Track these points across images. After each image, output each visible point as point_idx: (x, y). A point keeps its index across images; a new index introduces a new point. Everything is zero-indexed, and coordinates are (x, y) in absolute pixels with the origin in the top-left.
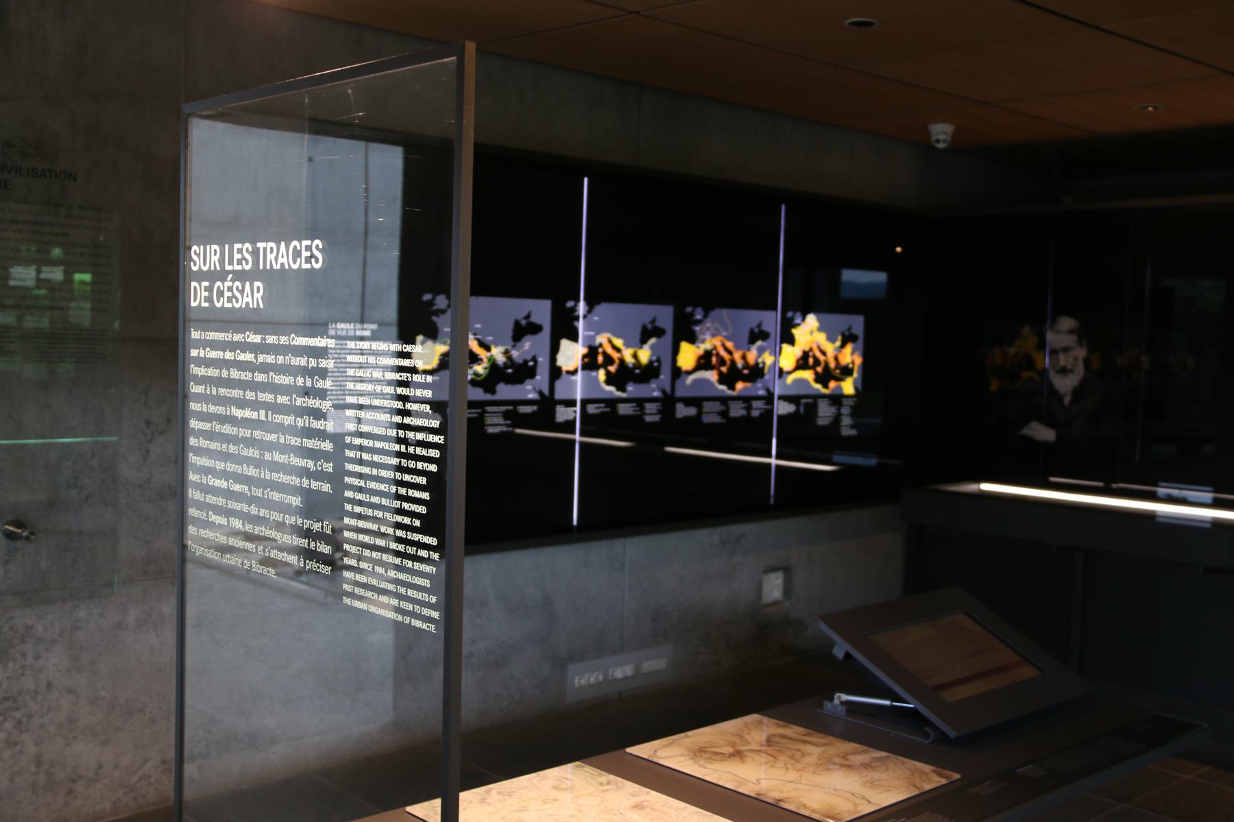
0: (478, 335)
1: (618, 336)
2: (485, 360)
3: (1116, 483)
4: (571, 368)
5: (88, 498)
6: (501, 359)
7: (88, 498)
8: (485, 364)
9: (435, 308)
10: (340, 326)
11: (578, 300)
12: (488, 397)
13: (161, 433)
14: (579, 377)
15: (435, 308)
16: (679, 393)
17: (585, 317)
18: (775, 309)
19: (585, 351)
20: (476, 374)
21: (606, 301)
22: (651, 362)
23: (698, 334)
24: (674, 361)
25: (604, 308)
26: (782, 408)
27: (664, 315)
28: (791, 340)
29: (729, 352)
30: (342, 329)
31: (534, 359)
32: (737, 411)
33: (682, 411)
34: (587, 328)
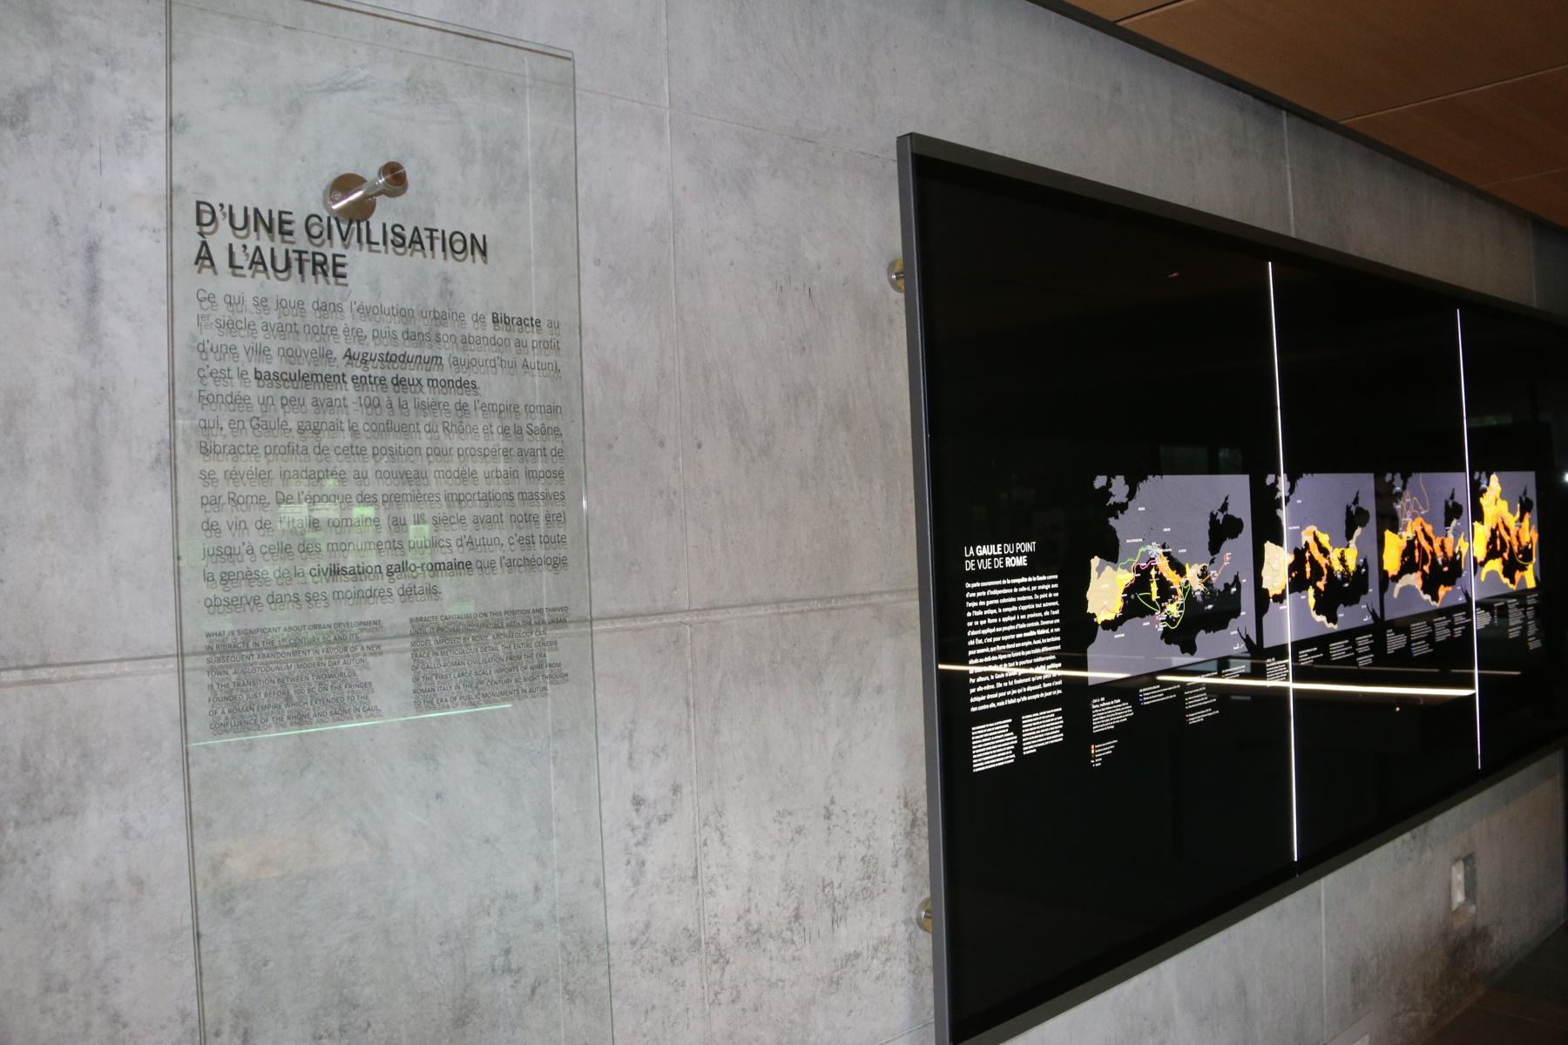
0: (1168, 548)
1: (1323, 532)
2: (1180, 592)
3: (1174, 698)
4: (1279, 592)
5: (533, 991)
6: (1197, 586)
7: (533, 991)
8: (1180, 600)
9: (1111, 501)
10: (983, 551)
11: (1277, 474)
12: (1186, 659)
13: (663, 820)
14: (1287, 606)
15: (1111, 501)
16: (1389, 615)
17: (1287, 499)
18: (1465, 471)
19: (1290, 558)
20: (1169, 620)
21: (1313, 471)
22: (1358, 567)
23: (1399, 515)
24: (1258, 579)
25: (1307, 481)
26: (1480, 620)
27: (1362, 485)
28: (1478, 515)
29: (1324, 552)
30: (985, 557)
31: (1237, 582)
32: (1442, 635)
33: (1395, 642)
34: (1292, 522)
